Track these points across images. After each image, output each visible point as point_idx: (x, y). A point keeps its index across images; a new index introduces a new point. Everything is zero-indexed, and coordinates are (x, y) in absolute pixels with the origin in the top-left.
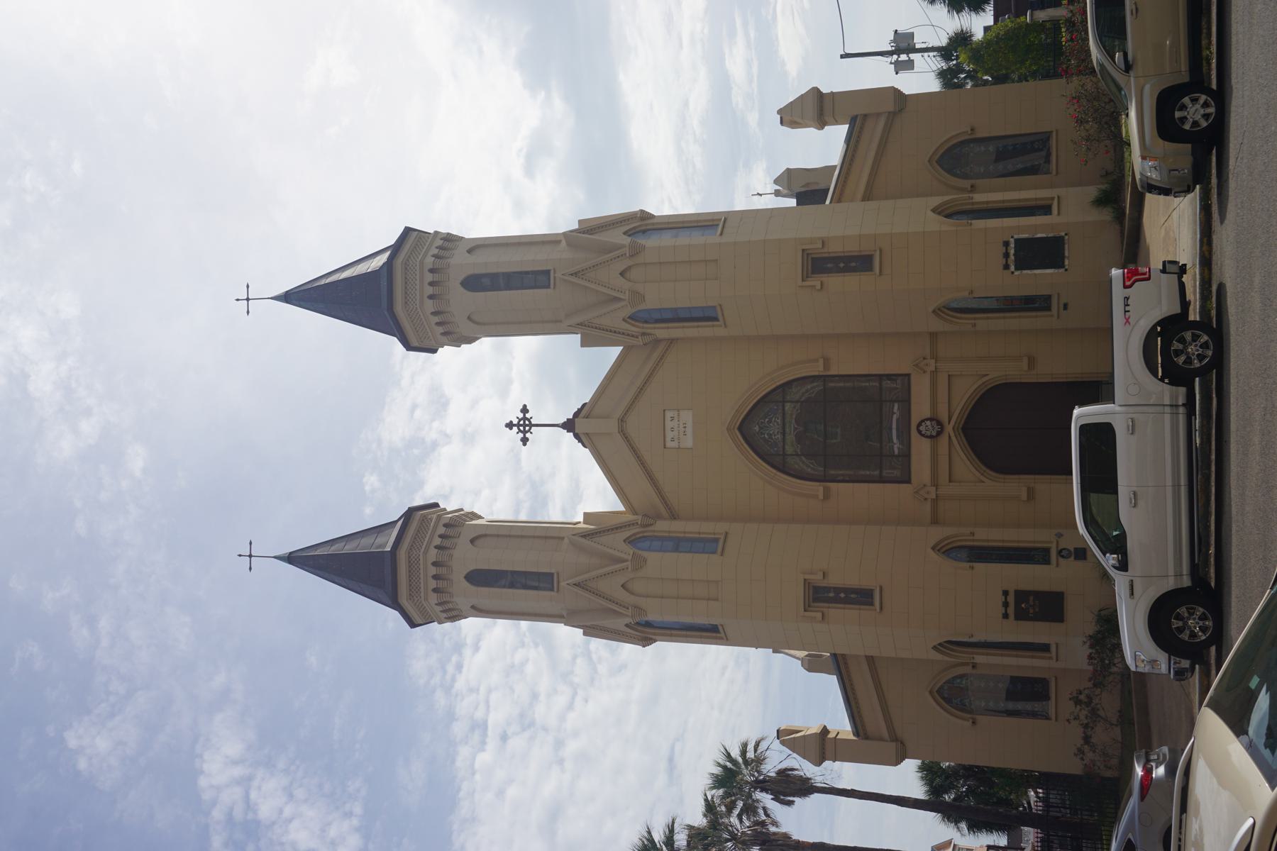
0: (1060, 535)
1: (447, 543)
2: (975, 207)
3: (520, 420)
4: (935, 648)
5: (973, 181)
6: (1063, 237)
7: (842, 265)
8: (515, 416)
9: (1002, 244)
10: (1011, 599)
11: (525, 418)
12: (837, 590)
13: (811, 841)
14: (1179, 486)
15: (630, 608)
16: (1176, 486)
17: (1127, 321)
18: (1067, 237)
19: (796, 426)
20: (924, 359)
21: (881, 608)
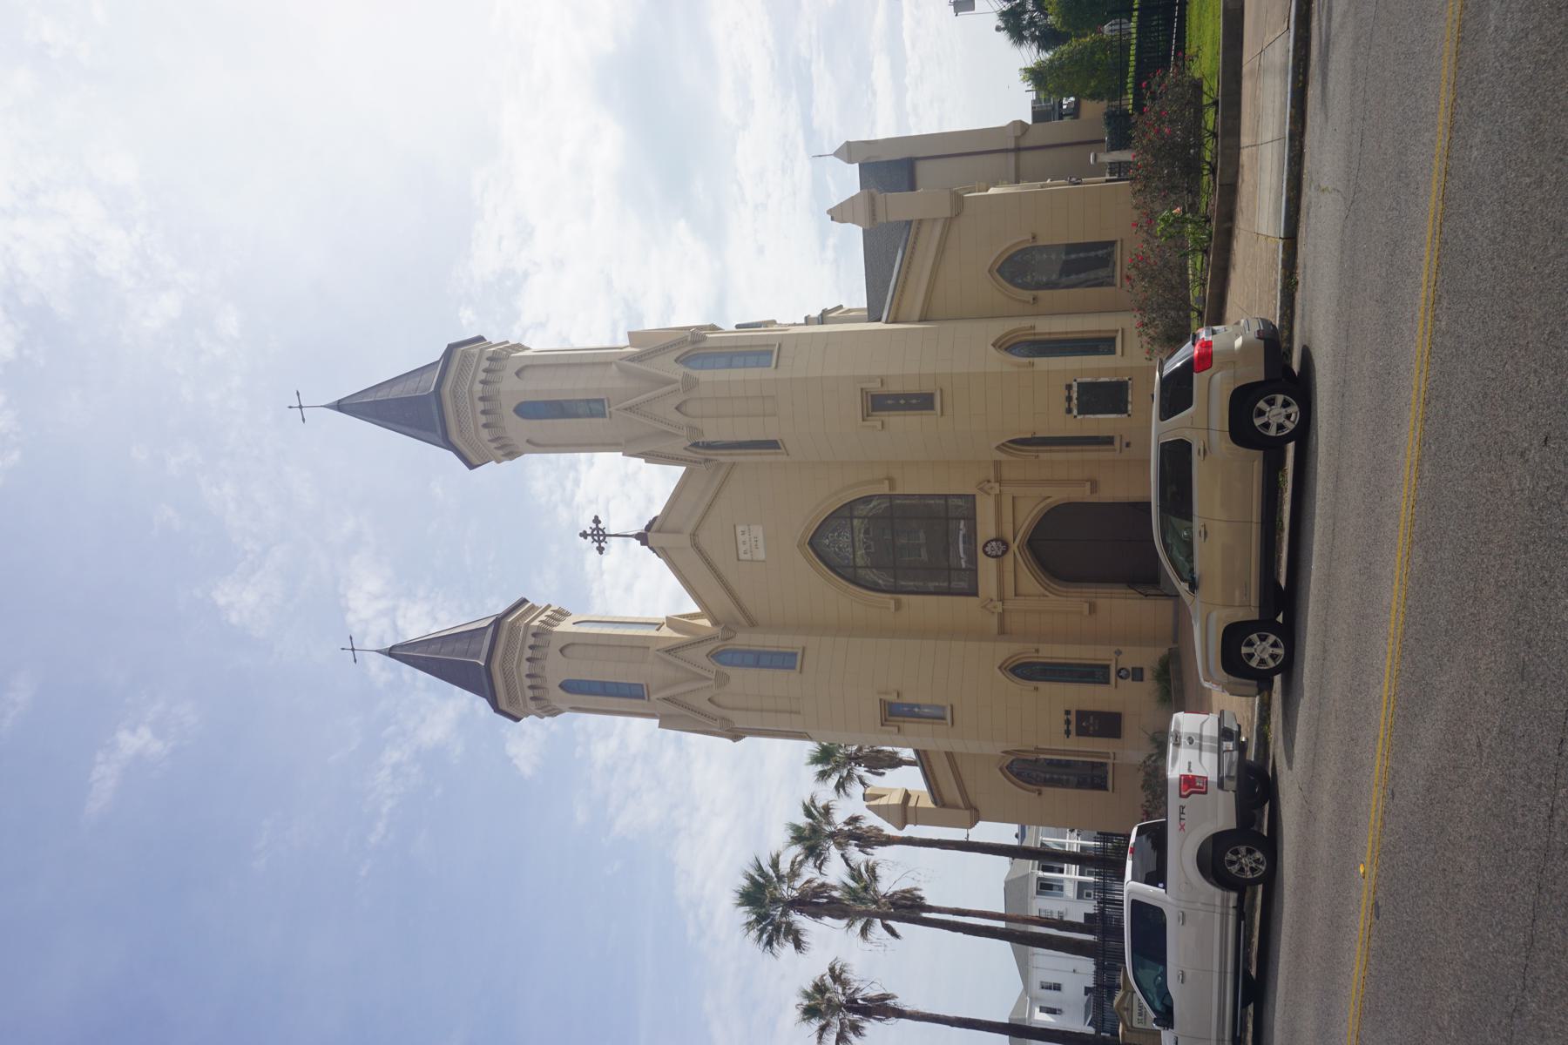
0: (1119, 653)
1: (538, 654)
2: (1037, 337)
3: (595, 540)
4: (998, 448)
5: (1035, 293)
6: (1127, 382)
7: (902, 402)
8: (588, 525)
9: (1064, 387)
10: (1073, 718)
11: (598, 529)
12: (896, 397)
13: (895, 846)
14: (1226, 972)
15: (685, 429)
16: (1223, 973)
17: (1182, 827)
18: (1130, 382)
20: (989, 481)
21: (953, 724)
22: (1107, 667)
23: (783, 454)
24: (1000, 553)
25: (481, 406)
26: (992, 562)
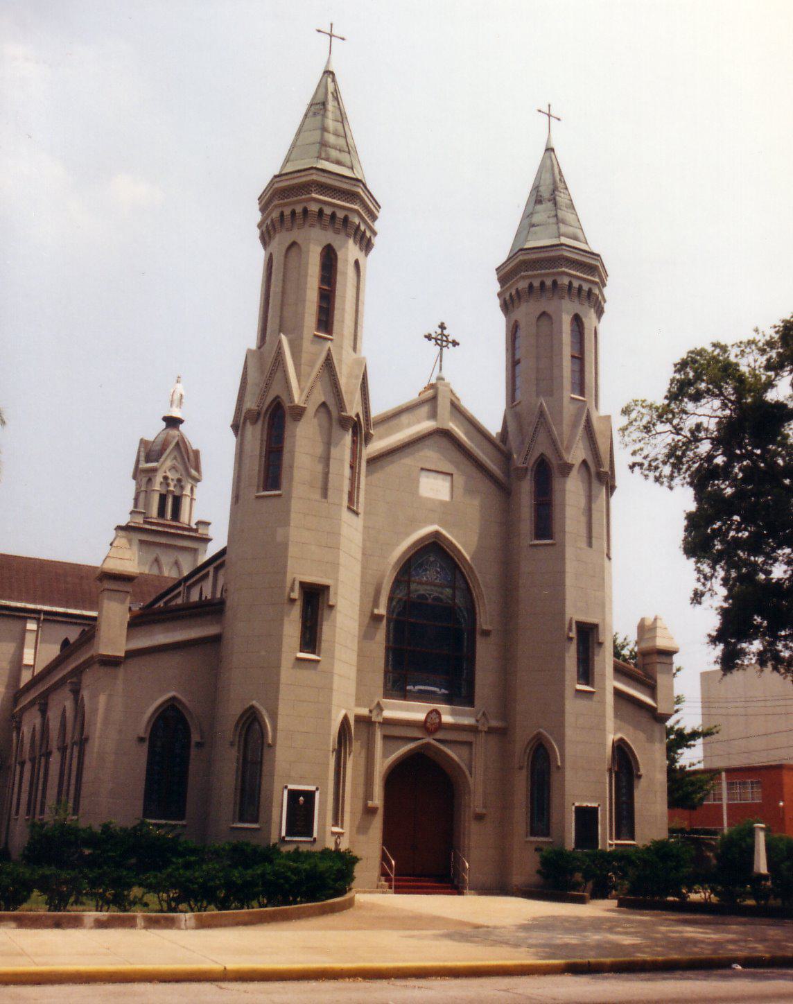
3: (446, 337)
8: (452, 333)
11: (442, 334)
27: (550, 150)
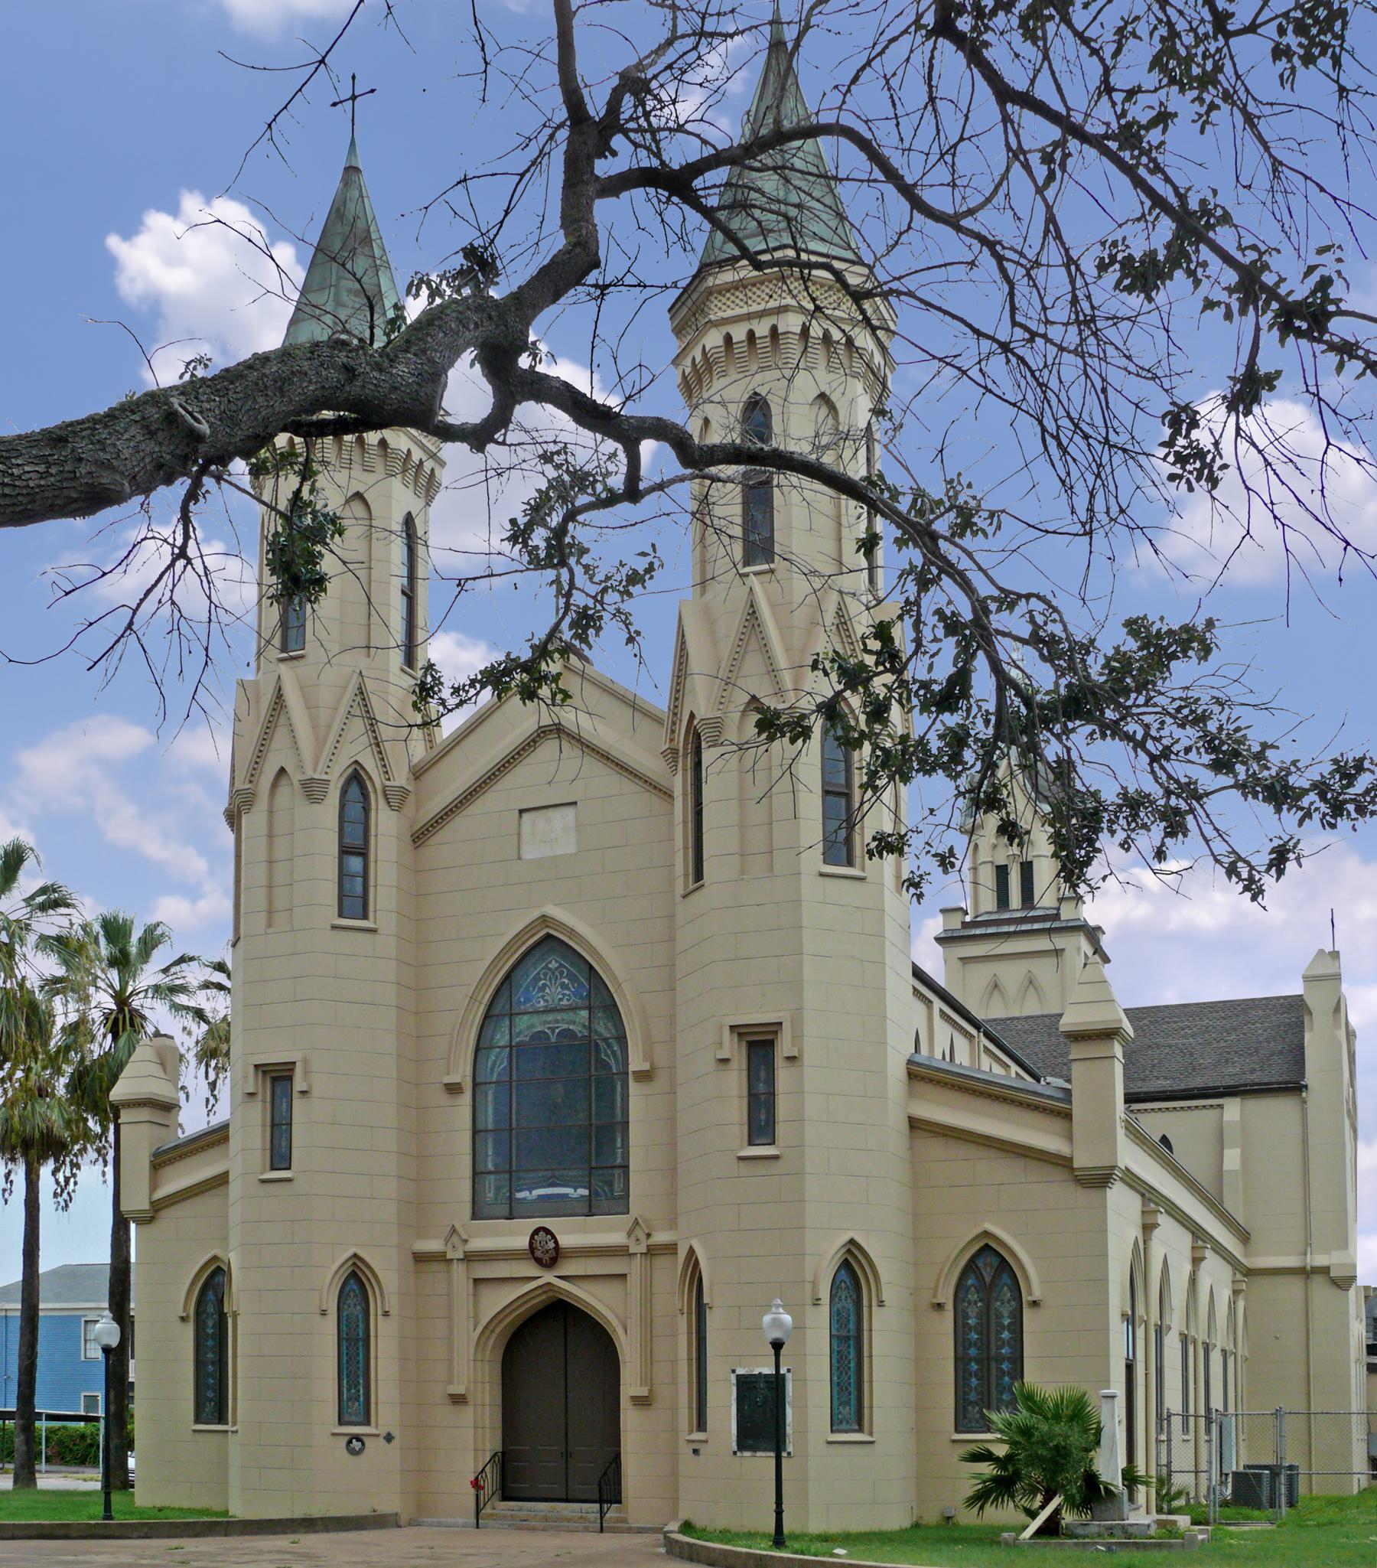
5: (950, 1306)
19: (557, 1031)
22: (367, 1423)
23: (686, 886)
24: (538, 1254)
25: (762, 329)
26: (523, 1242)
27: (351, 171)
